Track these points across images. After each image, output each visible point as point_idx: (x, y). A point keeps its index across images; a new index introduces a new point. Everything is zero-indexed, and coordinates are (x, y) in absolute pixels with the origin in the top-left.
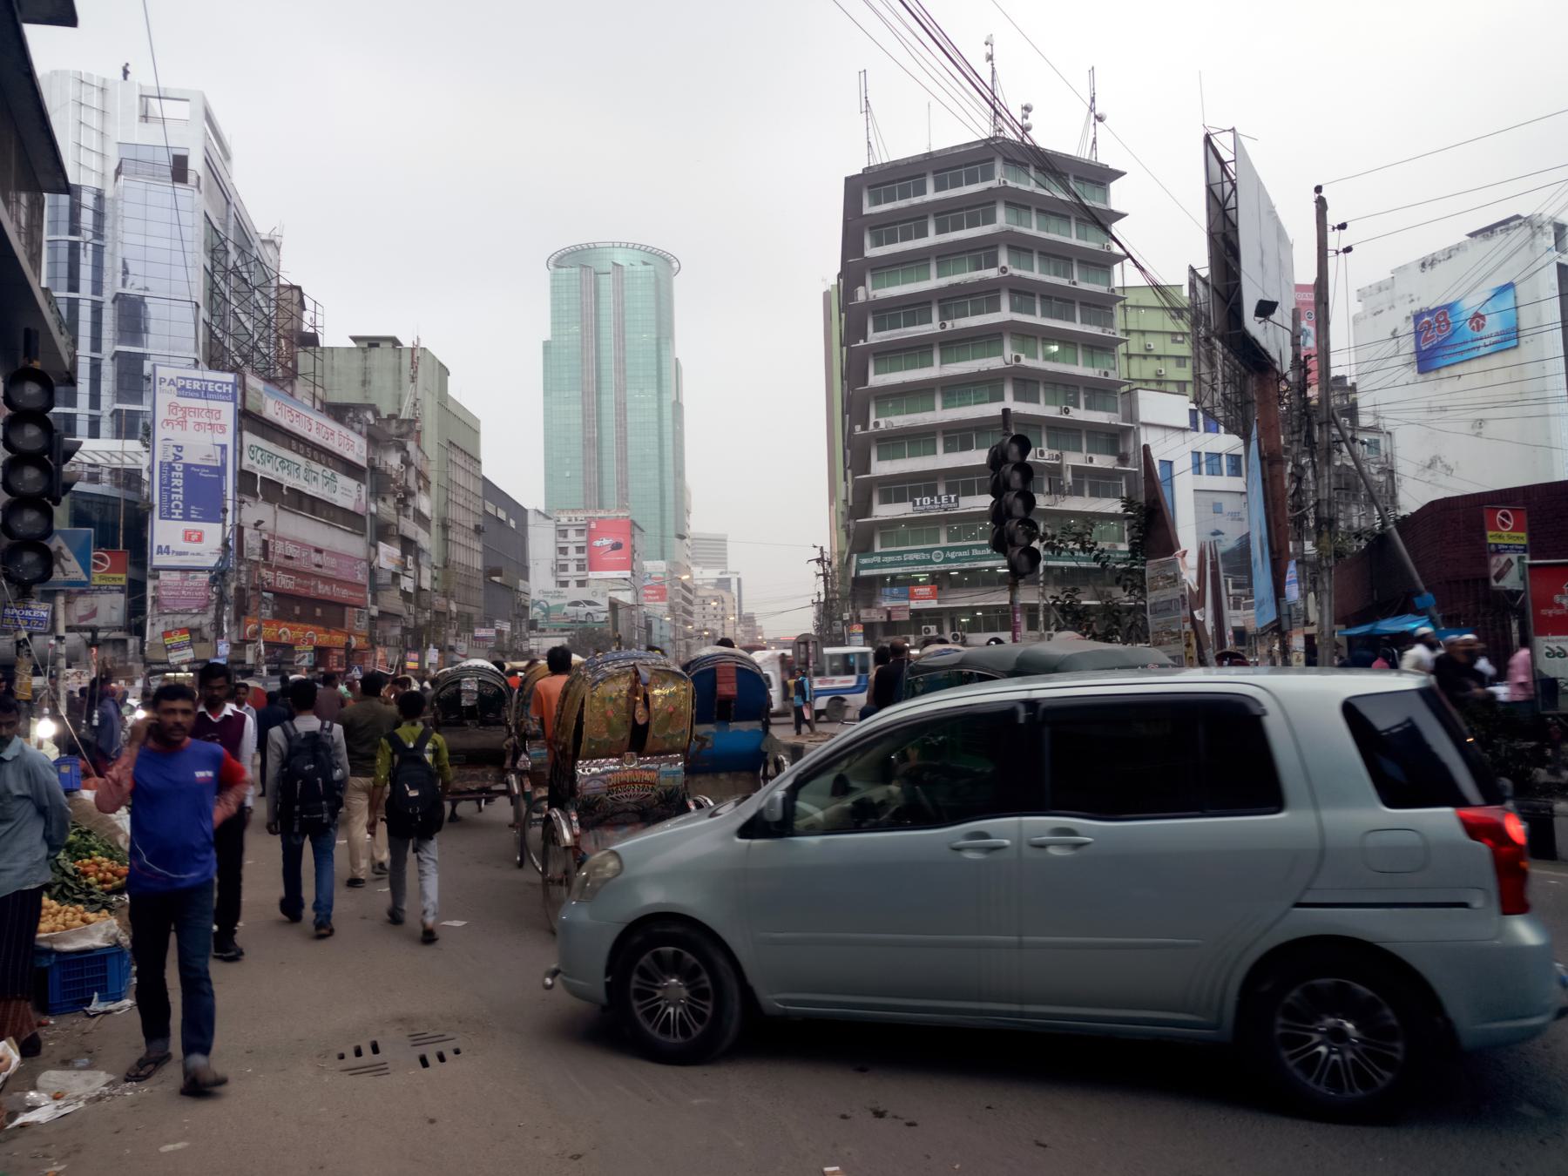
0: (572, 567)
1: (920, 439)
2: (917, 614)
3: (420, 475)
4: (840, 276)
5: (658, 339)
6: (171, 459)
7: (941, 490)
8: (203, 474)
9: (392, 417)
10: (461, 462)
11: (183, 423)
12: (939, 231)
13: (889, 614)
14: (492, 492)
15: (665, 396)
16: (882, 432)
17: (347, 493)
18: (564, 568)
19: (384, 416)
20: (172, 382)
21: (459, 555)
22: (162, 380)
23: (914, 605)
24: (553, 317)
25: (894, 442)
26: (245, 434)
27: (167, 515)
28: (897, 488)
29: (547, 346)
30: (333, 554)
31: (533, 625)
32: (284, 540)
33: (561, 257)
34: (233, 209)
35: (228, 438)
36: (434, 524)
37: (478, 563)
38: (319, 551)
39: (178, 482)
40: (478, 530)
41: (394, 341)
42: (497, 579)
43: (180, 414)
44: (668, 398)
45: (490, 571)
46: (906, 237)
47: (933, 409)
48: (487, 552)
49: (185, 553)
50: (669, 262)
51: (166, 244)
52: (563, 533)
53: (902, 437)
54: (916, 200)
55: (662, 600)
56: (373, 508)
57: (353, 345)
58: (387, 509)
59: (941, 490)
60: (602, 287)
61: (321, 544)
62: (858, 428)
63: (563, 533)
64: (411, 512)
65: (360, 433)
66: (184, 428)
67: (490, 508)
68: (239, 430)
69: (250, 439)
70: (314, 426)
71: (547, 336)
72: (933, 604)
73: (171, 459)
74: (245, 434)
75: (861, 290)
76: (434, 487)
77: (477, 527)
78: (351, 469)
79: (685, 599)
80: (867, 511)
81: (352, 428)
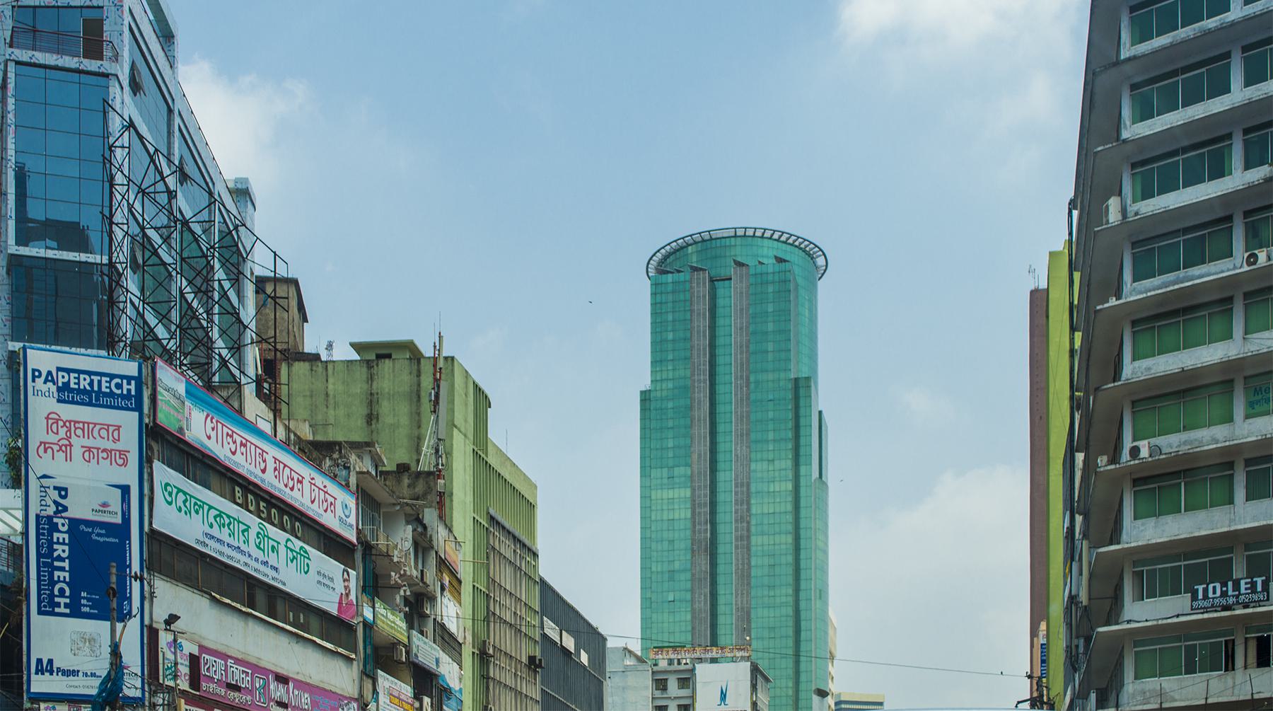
3: (443, 564)
4: (1072, 204)
6: (51, 510)
7: (1239, 570)
8: (98, 537)
9: (403, 468)
10: (508, 554)
11: (66, 448)
12: (1252, 79)
14: (554, 604)
16: (1144, 465)
17: (322, 582)
19: (389, 466)
20: (49, 378)
22: (36, 374)
24: (653, 352)
25: (1164, 483)
26: (157, 465)
27: (48, 608)
29: (645, 397)
30: (302, 685)
32: (225, 657)
34: (177, 120)
35: (130, 475)
36: (467, 651)
38: (282, 679)
39: (62, 550)
41: (410, 348)
43: (62, 432)
46: (1192, 98)
47: (1229, 419)
49: (75, 673)
51: (73, 170)
54: (1211, 23)
57: (356, 357)
58: (391, 622)
59: (1239, 570)
61: (286, 668)
62: (1102, 460)
63: (661, 684)
64: (429, 628)
66: (69, 458)
68: (145, 462)
69: (163, 473)
70: (271, 465)
71: (646, 382)
73: (51, 510)
74: (157, 465)
75: (1113, 204)
76: (466, 590)
77: (532, 659)
78: (331, 543)
80: (1113, 612)
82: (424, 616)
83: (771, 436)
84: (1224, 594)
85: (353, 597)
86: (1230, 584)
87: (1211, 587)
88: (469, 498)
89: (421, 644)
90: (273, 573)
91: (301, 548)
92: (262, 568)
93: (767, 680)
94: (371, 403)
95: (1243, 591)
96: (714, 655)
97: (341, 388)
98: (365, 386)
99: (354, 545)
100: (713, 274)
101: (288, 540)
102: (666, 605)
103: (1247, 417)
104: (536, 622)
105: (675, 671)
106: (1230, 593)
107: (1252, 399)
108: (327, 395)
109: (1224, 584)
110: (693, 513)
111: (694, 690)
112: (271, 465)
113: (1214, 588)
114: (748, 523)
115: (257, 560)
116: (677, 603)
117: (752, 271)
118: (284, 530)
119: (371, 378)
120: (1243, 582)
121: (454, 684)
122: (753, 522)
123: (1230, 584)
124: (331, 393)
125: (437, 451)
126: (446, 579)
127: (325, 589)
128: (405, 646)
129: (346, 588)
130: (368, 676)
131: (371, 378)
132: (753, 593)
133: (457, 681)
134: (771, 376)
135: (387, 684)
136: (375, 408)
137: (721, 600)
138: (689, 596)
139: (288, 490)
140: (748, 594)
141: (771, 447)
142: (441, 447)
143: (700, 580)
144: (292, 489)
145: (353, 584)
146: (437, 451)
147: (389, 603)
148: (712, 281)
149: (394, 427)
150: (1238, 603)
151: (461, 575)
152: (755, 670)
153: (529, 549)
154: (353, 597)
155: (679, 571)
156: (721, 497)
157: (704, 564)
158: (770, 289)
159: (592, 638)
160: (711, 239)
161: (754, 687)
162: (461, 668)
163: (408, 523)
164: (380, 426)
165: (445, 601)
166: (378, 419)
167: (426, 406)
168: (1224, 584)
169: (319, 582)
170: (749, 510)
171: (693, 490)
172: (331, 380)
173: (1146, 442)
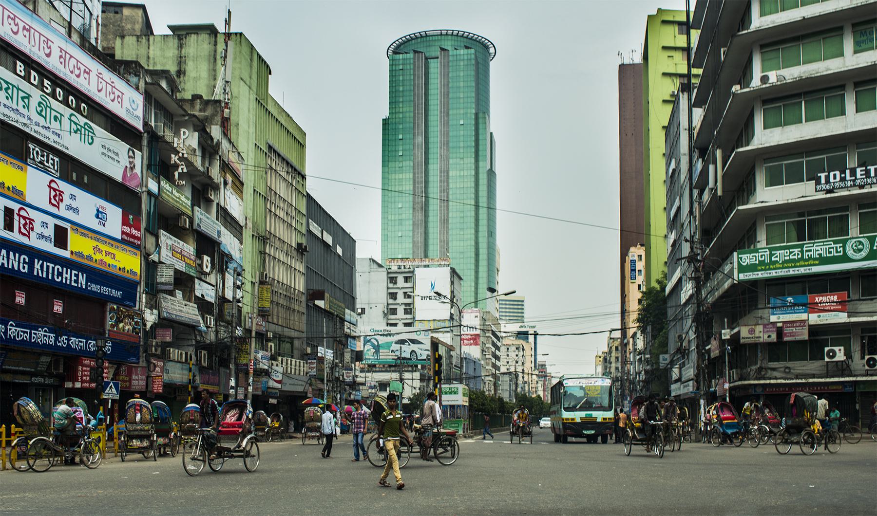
0: (401, 310)
1: (823, 93)
2: (815, 330)
3: (226, 167)
5: (476, 115)
13: (780, 332)
15: (481, 164)
16: (774, 87)
17: (112, 158)
18: (394, 311)
21: (280, 274)
23: (814, 319)
28: (788, 162)
31: (358, 356)
33: (399, 46)
36: (247, 234)
37: (300, 284)
40: (301, 249)
42: (320, 303)
44: (484, 166)
45: (314, 294)
48: (310, 273)
50: (486, 47)
52: (393, 280)
53: (798, 95)
55: (476, 344)
56: (153, 186)
58: (180, 198)
59: (852, 161)
60: (431, 70)
63: (393, 280)
65: (137, 89)
67: (315, 229)
70: (56, 53)
71: (386, 114)
72: (842, 318)
76: (248, 190)
77: (299, 245)
79: (494, 344)
81: (128, 82)
82: (209, 201)
83: (462, 144)
84: (843, 179)
85: (138, 170)
86: (848, 172)
87: (832, 174)
88: (252, 130)
89: (204, 218)
90: (56, 138)
91: (86, 124)
92: (43, 131)
93: (460, 279)
94: (180, 64)
95: (858, 176)
96: (427, 263)
97: (158, 53)
98: (176, 52)
99: (141, 133)
100: (427, 55)
101: (72, 115)
102: (397, 239)
103: (855, 52)
104: (304, 222)
105: (402, 273)
106: (848, 178)
107: (859, 39)
108: (148, 57)
109: (843, 172)
110: (414, 187)
111: (414, 283)
112: (56, 53)
113: (835, 176)
114: (448, 193)
115: (37, 124)
116: (404, 238)
117: (451, 53)
118: (69, 106)
119: (181, 46)
120: (858, 170)
121: (236, 255)
122: (451, 192)
123: (848, 172)
124: (151, 56)
125: (225, 90)
126: (230, 179)
127: (110, 160)
128: (189, 217)
129: (130, 163)
130: (152, 234)
131: (181, 46)
132: (450, 232)
133: (238, 252)
134: (462, 112)
135: (170, 242)
136: (183, 66)
137: (431, 236)
138: (411, 234)
139: (73, 76)
140: (448, 233)
141: (462, 151)
142: (227, 88)
143: (418, 225)
144: (78, 76)
145: (138, 161)
146: (225, 90)
147: (170, 179)
148: (427, 59)
149: (196, 79)
150: (854, 185)
151: (243, 177)
152: (453, 272)
153: (299, 174)
154: (138, 170)
155: (405, 220)
156: (431, 179)
157: (421, 216)
158: (462, 63)
159: (349, 242)
160: (427, 36)
161: (452, 283)
162: (241, 243)
163: (195, 131)
164: (186, 78)
165: (228, 193)
166: (185, 73)
167: (219, 61)
168: (843, 172)
169: (103, 154)
170: (448, 185)
171: (414, 174)
172: (151, 48)
173: (774, 72)
